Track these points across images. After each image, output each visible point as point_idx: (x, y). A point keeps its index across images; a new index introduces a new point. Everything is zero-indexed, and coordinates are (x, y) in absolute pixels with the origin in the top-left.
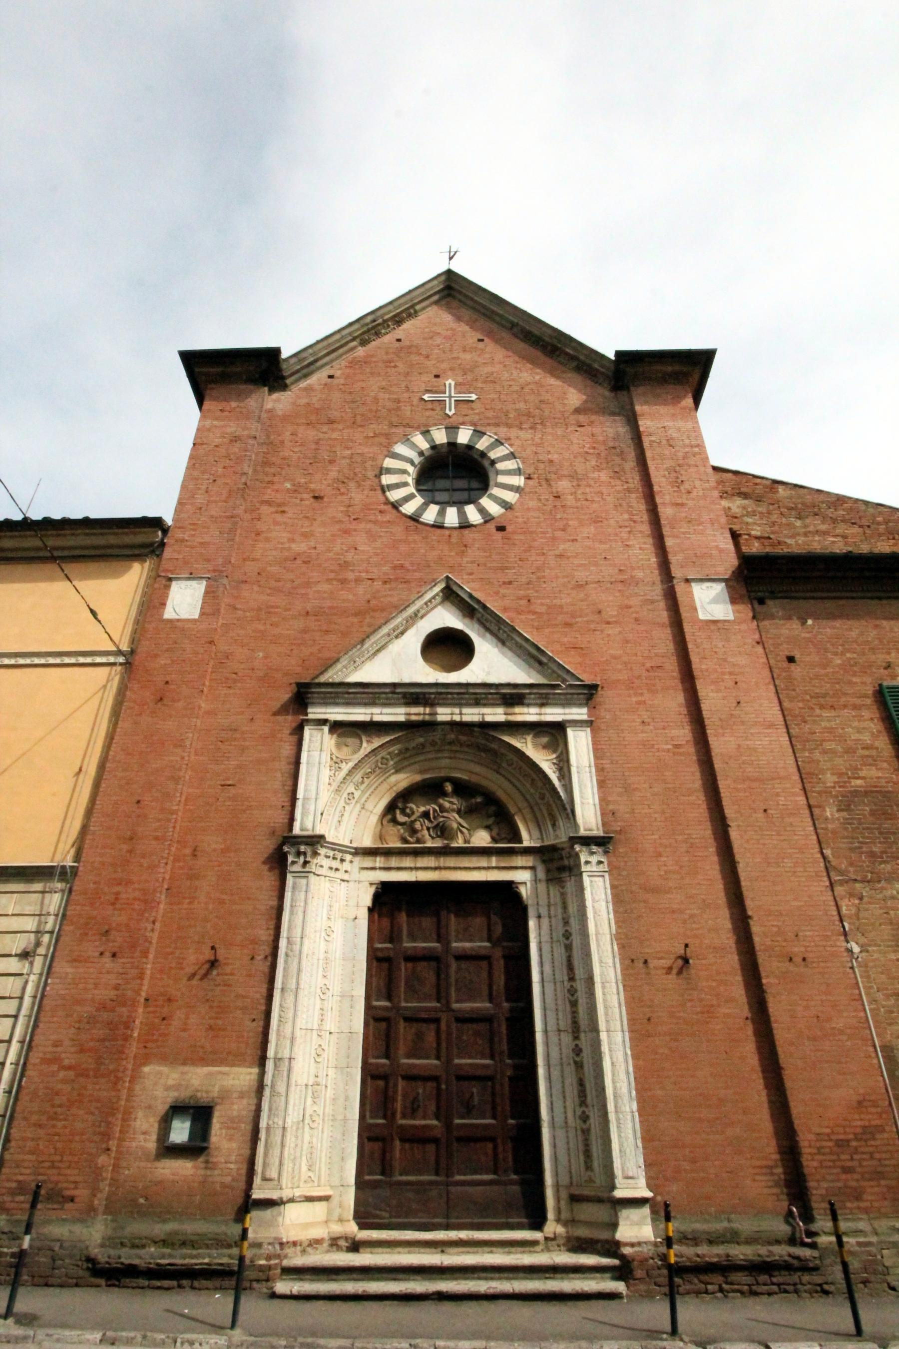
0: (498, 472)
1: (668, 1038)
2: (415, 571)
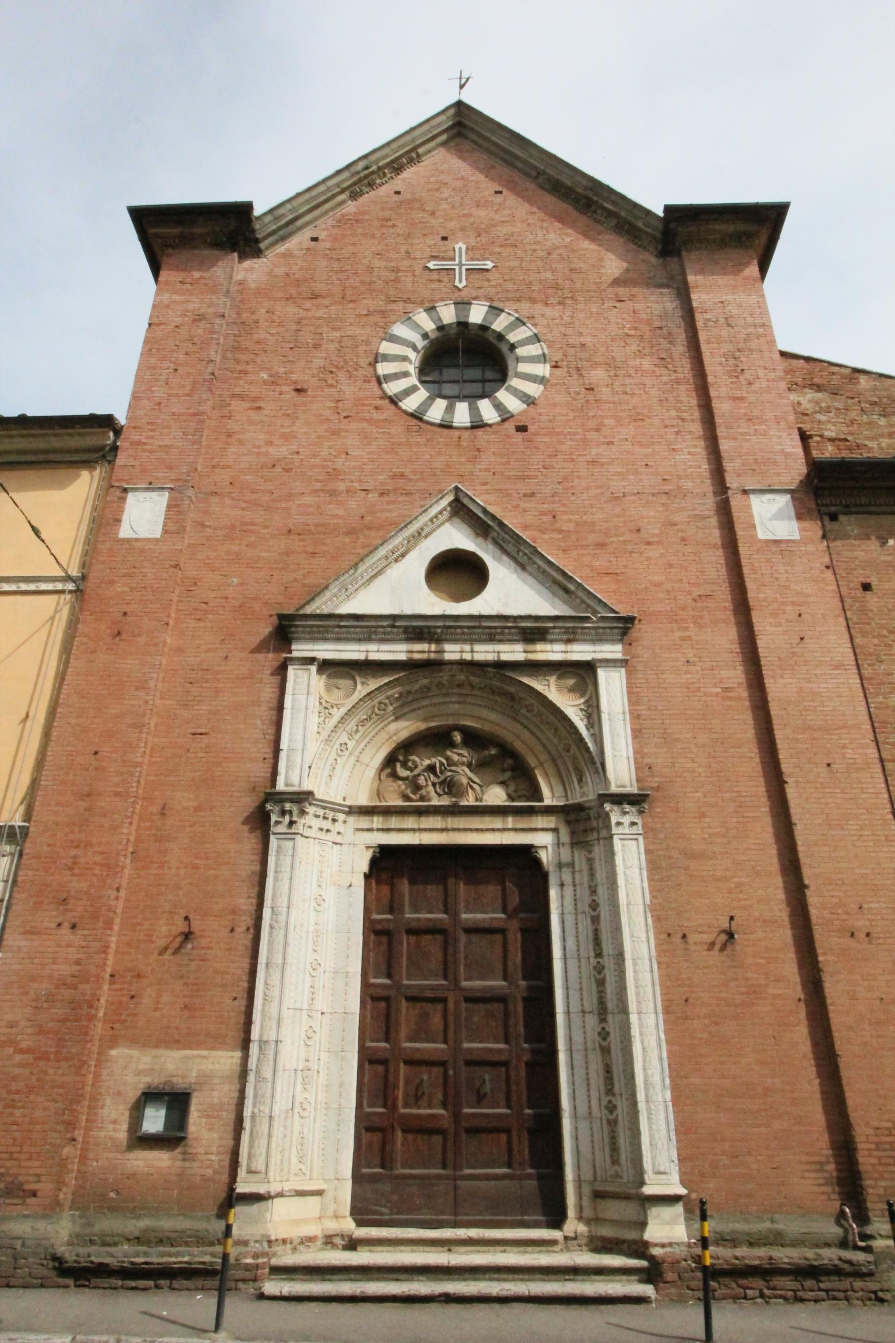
0: (518, 359)
1: (707, 1021)
2: (417, 480)
